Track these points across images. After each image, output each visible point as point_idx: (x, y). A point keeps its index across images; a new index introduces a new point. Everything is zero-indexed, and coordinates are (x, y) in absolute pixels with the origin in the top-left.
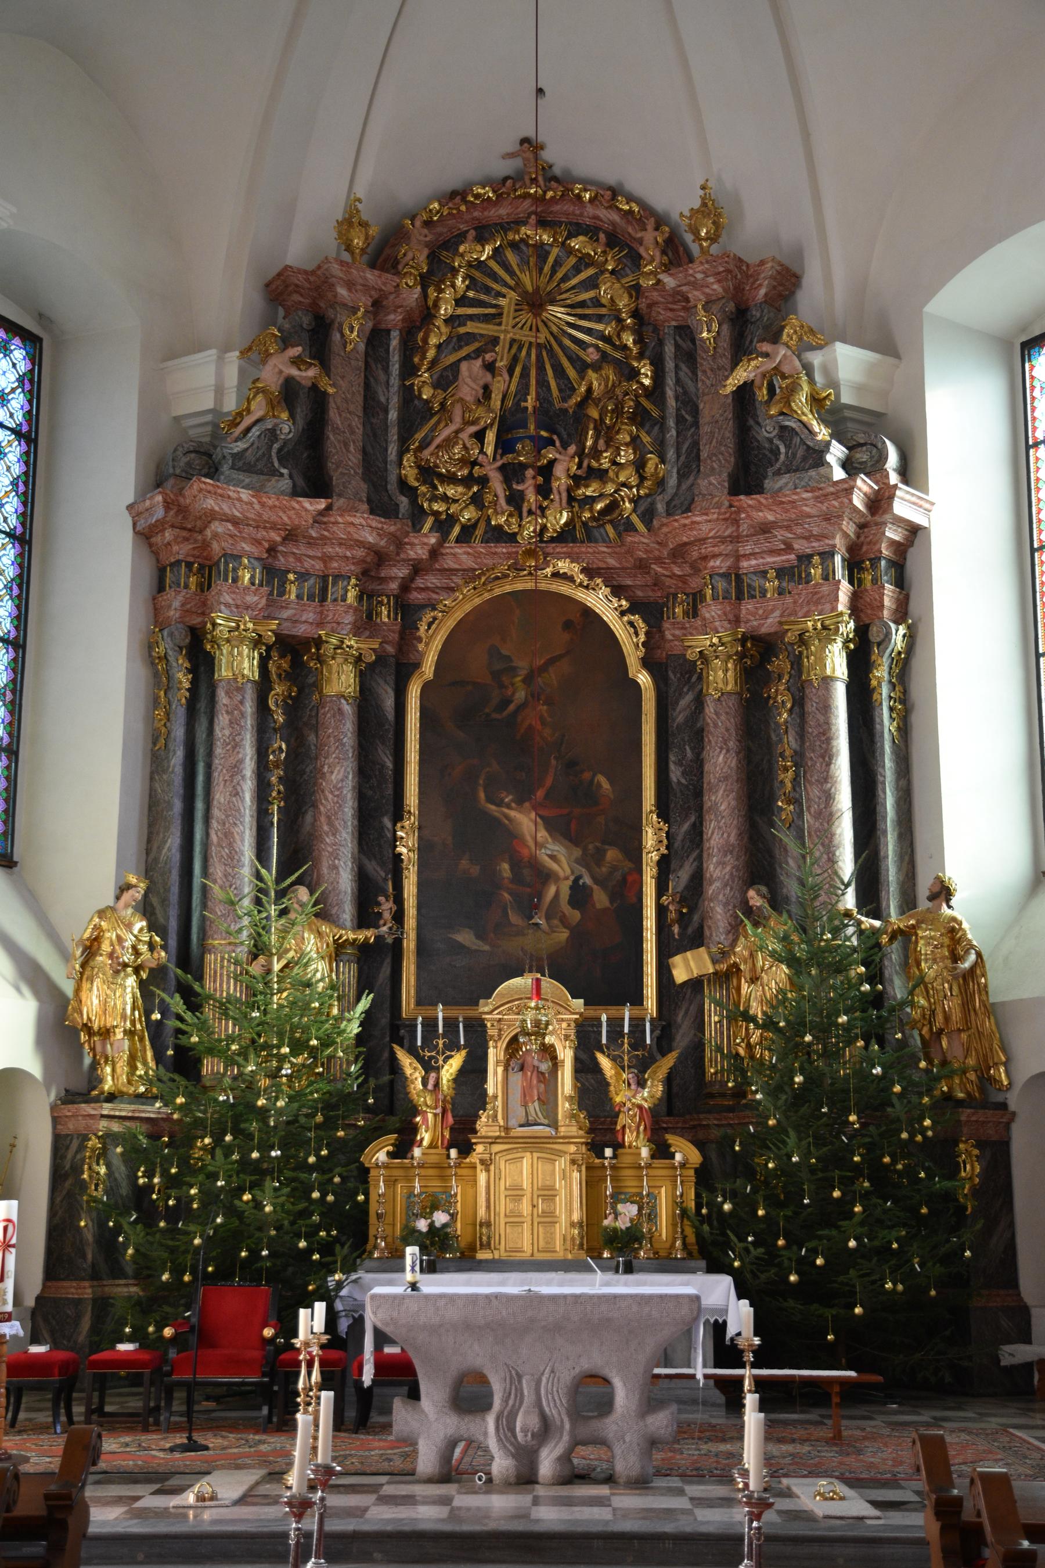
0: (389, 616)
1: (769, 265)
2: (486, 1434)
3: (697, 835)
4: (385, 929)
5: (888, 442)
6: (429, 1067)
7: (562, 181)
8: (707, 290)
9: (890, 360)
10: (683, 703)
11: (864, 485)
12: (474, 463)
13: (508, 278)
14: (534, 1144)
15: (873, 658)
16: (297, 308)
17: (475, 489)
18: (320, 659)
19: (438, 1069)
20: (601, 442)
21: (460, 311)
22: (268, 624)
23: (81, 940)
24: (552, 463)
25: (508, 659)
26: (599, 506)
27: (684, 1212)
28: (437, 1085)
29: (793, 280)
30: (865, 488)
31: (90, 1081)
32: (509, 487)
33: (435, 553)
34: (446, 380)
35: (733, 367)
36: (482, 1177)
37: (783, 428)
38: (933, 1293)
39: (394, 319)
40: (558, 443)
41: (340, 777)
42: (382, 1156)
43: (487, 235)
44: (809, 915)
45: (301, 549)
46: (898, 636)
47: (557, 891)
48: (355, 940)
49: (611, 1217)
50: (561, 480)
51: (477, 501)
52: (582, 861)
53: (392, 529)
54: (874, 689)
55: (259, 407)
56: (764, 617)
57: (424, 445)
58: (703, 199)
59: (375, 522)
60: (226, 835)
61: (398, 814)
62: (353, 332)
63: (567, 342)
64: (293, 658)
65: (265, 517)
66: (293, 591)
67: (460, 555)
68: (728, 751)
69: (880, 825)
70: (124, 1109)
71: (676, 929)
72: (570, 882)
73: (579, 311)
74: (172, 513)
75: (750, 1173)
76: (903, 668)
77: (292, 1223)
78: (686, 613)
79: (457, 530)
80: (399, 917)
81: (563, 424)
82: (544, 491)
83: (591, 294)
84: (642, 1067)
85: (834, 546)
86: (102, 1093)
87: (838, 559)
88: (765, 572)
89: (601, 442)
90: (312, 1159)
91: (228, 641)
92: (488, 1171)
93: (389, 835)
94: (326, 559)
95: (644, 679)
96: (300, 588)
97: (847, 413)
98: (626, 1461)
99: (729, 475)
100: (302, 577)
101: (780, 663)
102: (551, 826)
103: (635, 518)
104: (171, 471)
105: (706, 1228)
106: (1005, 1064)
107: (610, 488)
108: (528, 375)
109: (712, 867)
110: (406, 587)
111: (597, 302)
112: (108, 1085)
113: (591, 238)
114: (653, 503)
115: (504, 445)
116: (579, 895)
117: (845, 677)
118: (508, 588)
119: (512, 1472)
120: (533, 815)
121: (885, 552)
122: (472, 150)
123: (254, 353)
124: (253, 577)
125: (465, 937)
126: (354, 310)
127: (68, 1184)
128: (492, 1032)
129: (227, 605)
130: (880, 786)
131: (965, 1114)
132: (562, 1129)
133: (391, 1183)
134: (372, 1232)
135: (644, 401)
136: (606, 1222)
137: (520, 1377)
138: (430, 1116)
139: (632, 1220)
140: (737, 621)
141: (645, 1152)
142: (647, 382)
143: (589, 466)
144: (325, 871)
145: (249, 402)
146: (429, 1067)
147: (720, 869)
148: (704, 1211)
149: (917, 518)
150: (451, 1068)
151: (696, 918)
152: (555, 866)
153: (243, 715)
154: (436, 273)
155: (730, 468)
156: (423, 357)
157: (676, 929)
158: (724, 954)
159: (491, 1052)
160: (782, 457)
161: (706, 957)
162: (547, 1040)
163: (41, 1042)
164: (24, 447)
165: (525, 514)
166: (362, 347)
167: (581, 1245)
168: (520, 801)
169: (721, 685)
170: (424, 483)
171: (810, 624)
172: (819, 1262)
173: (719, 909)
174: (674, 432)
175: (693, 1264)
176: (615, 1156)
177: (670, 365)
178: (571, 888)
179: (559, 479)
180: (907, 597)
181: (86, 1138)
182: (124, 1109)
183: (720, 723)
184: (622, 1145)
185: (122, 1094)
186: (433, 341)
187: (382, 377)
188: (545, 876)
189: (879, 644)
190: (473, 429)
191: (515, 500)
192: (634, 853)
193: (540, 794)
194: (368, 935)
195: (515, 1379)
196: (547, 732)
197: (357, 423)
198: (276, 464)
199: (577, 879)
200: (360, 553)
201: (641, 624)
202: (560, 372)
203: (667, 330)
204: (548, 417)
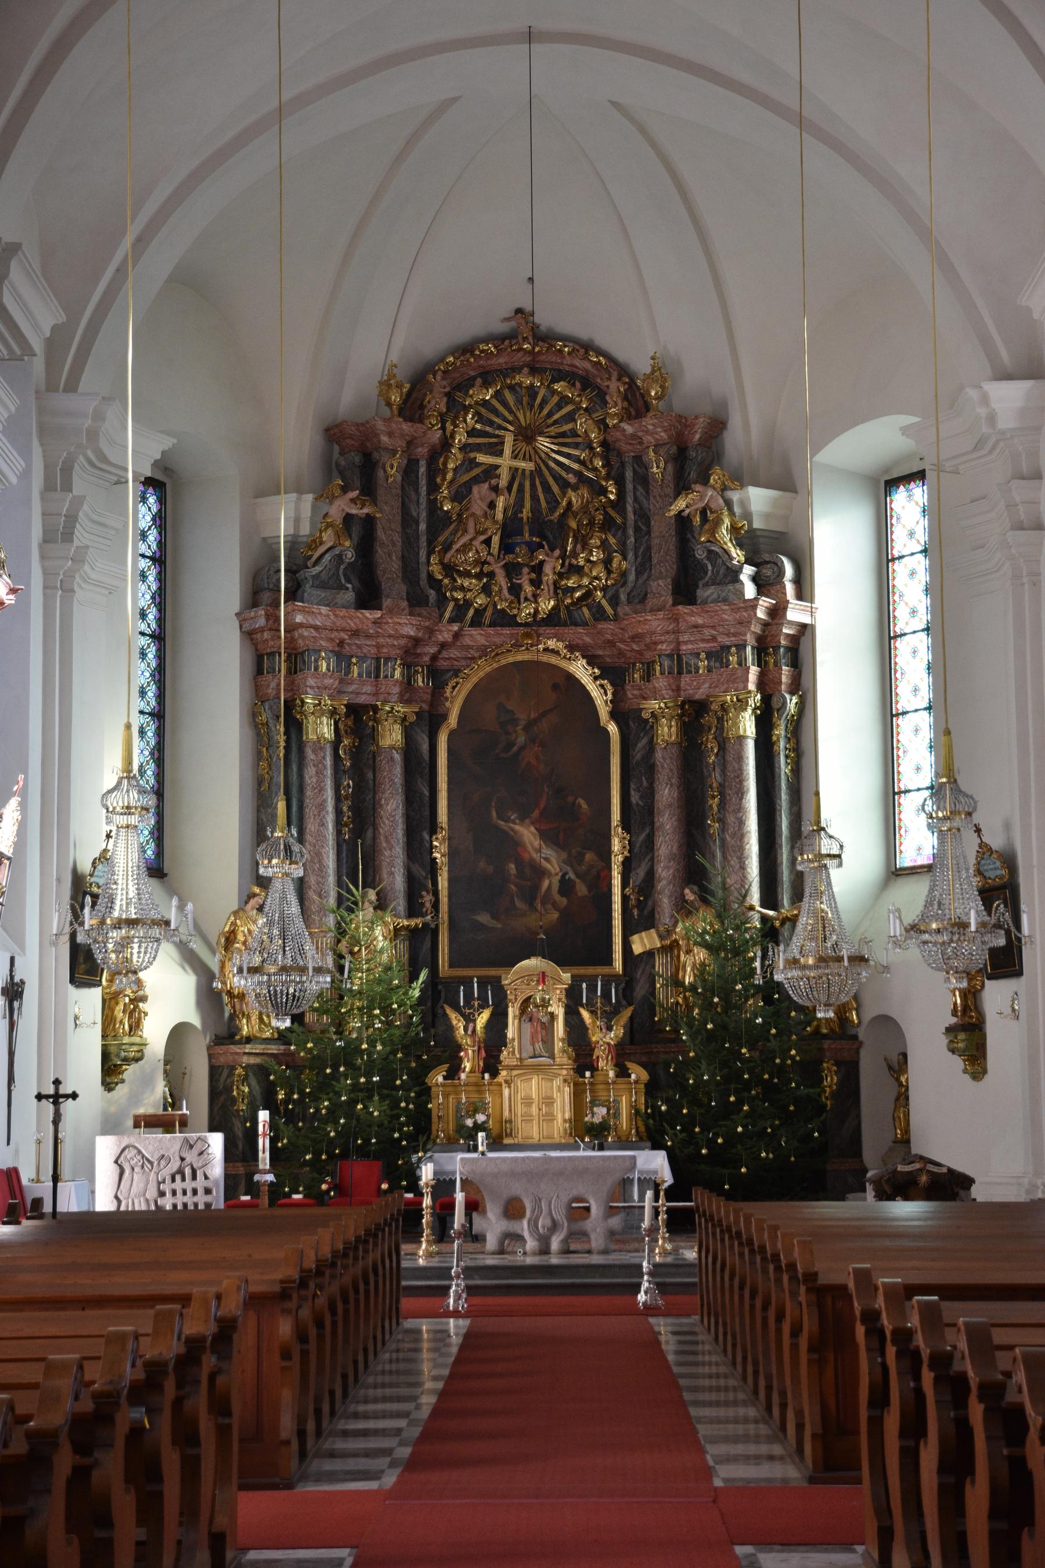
0: (423, 682)
1: (702, 420)
2: (523, 1229)
4: (429, 917)
5: (784, 559)
6: (469, 1019)
7: (545, 338)
8: (656, 436)
9: (787, 494)
10: (640, 745)
11: (765, 602)
13: (506, 414)
14: (537, 1069)
15: (774, 720)
16: (349, 456)
17: (485, 580)
18: (377, 721)
19: (474, 1021)
20: (579, 546)
21: (471, 441)
22: (341, 700)
23: (223, 933)
25: (512, 712)
26: (578, 594)
27: (637, 1112)
28: (474, 1031)
30: (766, 604)
31: (229, 1028)
32: (510, 580)
33: (457, 636)
34: (461, 495)
35: (676, 498)
36: (506, 1092)
37: (710, 552)
38: (793, 1159)
39: (422, 451)
40: (546, 547)
41: (394, 806)
42: (440, 1079)
43: (490, 379)
44: (728, 910)
46: (792, 703)
47: (550, 884)
48: (408, 926)
49: (589, 1116)
50: (549, 576)
51: (486, 590)
52: (568, 862)
53: (427, 624)
54: (774, 743)
57: (447, 548)
58: (653, 367)
59: (415, 620)
60: (316, 854)
61: (434, 828)
62: (392, 470)
63: (552, 464)
64: (358, 721)
65: (338, 623)
67: (476, 637)
68: (671, 786)
69: (778, 840)
70: (258, 1048)
71: (636, 912)
72: (559, 877)
73: (561, 440)
74: (271, 622)
75: (683, 1087)
77: (390, 1122)
78: (642, 678)
79: (471, 612)
80: (436, 905)
81: (549, 532)
82: (536, 583)
83: (570, 426)
84: (609, 1017)
85: (746, 641)
86: (242, 1038)
87: (749, 649)
88: (699, 654)
89: (579, 546)
90: (398, 1082)
91: (313, 713)
92: (509, 1087)
93: (428, 845)
94: (378, 647)
95: (612, 728)
97: (758, 533)
98: (597, 1241)
99: (673, 580)
101: (708, 719)
102: (543, 835)
103: (604, 602)
104: (266, 585)
105: (651, 1121)
106: (857, 1010)
107: (585, 581)
108: (523, 491)
109: (660, 870)
110: (434, 658)
111: (574, 433)
112: (245, 1031)
113: (569, 382)
114: (617, 591)
115: (506, 548)
116: (566, 887)
117: (754, 735)
118: (511, 660)
119: (537, 1248)
120: (532, 829)
121: (783, 642)
122: (483, 315)
123: (324, 495)
124: (328, 665)
125: (484, 918)
126: (394, 452)
127: (222, 1099)
128: (510, 997)
129: (311, 687)
130: (778, 813)
131: (826, 1044)
132: (558, 1060)
133: (446, 1096)
134: (434, 1127)
135: (610, 510)
136: (586, 1119)
137: (540, 1200)
138: (470, 1052)
139: (603, 1117)
140: (678, 689)
141: (611, 1074)
142: (612, 497)
144: (385, 876)
145: (321, 533)
147: (665, 872)
148: (649, 1111)
150: (483, 1018)
151: (650, 903)
152: (548, 866)
153: (325, 767)
154: (455, 409)
155: (673, 573)
156: (444, 479)
157: (636, 912)
158: (669, 932)
159: (510, 1010)
160: (710, 573)
161: (655, 936)
162: (549, 1009)
163: (199, 1004)
164: (157, 723)
165: (522, 600)
166: (399, 478)
167: (571, 1134)
168: (522, 819)
169: (666, 738)
170: (446, 576)
171: (729, 698)
172: (720, 1141)
173: (665, 900)
174: (632, 539)
175: (643, 1144)
176: (592, 1076)
177: (629, 486)
178: (560, 881)
179: (548, 575)
180: (800, 674)
181: (233, 1068)
182: (258, 1048)
183: (666, 764)
184: (597, 1069)
185: (256, 1038)
186: (451, 466)
187: (414, 496)
188: (541, 873)
189: (778, 710)
190: (482, 538)
191: (515, 590)
192: (606, 855)
193: (536, 814)
194: (418, 922)
195: (537, 1201)
197: (397, 538)
198: (343, 581)
199: (564, 876)
201: (609, 687)
202: (547, 488)
203: (628, 458)
204: (538, 525)
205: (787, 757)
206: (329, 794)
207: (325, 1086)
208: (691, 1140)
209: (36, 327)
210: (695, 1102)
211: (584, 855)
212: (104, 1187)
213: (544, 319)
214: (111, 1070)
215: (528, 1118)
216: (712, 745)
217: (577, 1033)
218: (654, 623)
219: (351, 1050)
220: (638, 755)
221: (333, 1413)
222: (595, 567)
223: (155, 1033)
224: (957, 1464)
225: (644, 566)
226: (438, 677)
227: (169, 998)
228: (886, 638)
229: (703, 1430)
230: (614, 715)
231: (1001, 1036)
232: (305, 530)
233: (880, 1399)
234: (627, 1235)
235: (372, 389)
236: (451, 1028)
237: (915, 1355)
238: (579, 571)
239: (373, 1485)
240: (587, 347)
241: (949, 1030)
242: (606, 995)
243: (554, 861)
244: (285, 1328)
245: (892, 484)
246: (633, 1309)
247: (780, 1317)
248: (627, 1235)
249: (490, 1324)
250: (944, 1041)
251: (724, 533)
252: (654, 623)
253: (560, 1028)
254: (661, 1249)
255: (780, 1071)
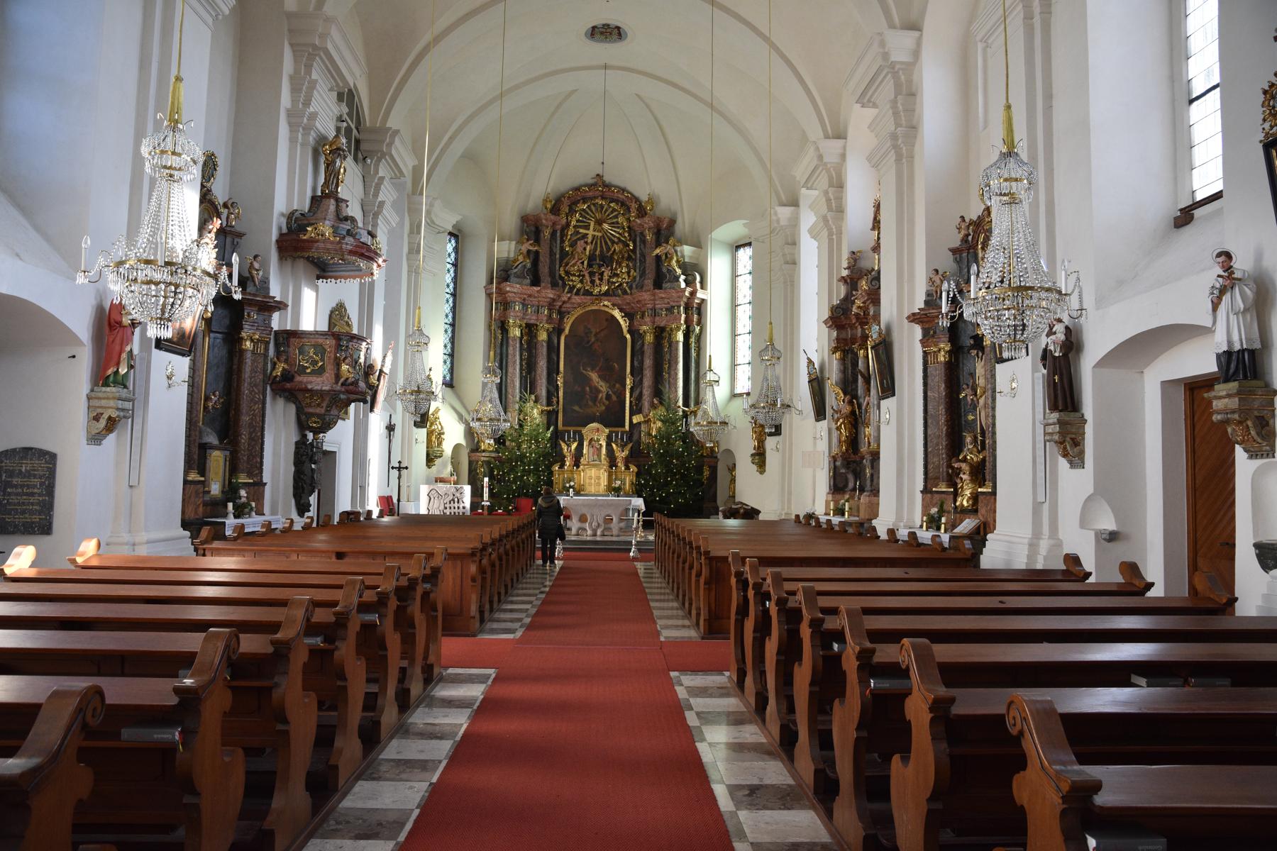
3: (641, 381)
6: (569, 446)
7: (607, 186)
11: (689, 289)
14: (594, 466)
16: (530, 227)
34: (573, 245)
39: (559, 227)
44: (671, 407)
46: (697, 329)
47: (602, 396)
50: (606, 277)
51: (581, 282)
55: (521, 258)
56: (661, 322)
62: (547, 233)
64: (530, 330)
67: (577, 299)
75: (650, 474)
76: (700, 338)
81: (606, 260)
82: (601, 279)
84: (623, 447)
95: (628, 336)
98: (615, 532)
102: (600, 377)
115: (590, 265)
116: (608, 397)
122: (581, 174)
123: (519, 242)
125: (576, 408)
146: (569, 446)
147: (647, 393)
150: (574, 446)
154: (572, 211)
188: (599, 391)
191: (593, 282)
192: (624, 385)
204: (603, 257)
206: (518, 357)
207: (512, 469)
208: (653, 494)
209: (405, 165)
210: (654, 480)
212: (422, 503)
213: (607, 179)
214: (430, 460)
215: (590, 484)
216: (666, 344)
217: (610, 453)
218: (646, 296)
219: (523, 456)
220: (638, 347)
221: (499, 601)
222: (623, 274)
223: (447, 448)
224: (791, 650)
225: (643, 274)
226: (562, 314)
227: (453, 434)
228: (734, 306)
229: (656, 613)
230: (629, 331)
231: (772, 458)
232: (512, 255)
233: (743, 611)
234: (627, 529)
235: (540, 202)
236: (562, 449)
237: (746, 582)
238: (617, 275)
239: (511, 636)
240: (624, 190)
242: (622, 439)
244: (473, 569)
245: (738, 247)
246: (628, 559)
247: (691, 567)
248: (627, 529)
249: (571, 563)
251: (674, 263)
252: (646, 296)
253: (604, 450)
254: (639, 536)
255: (688, 469)
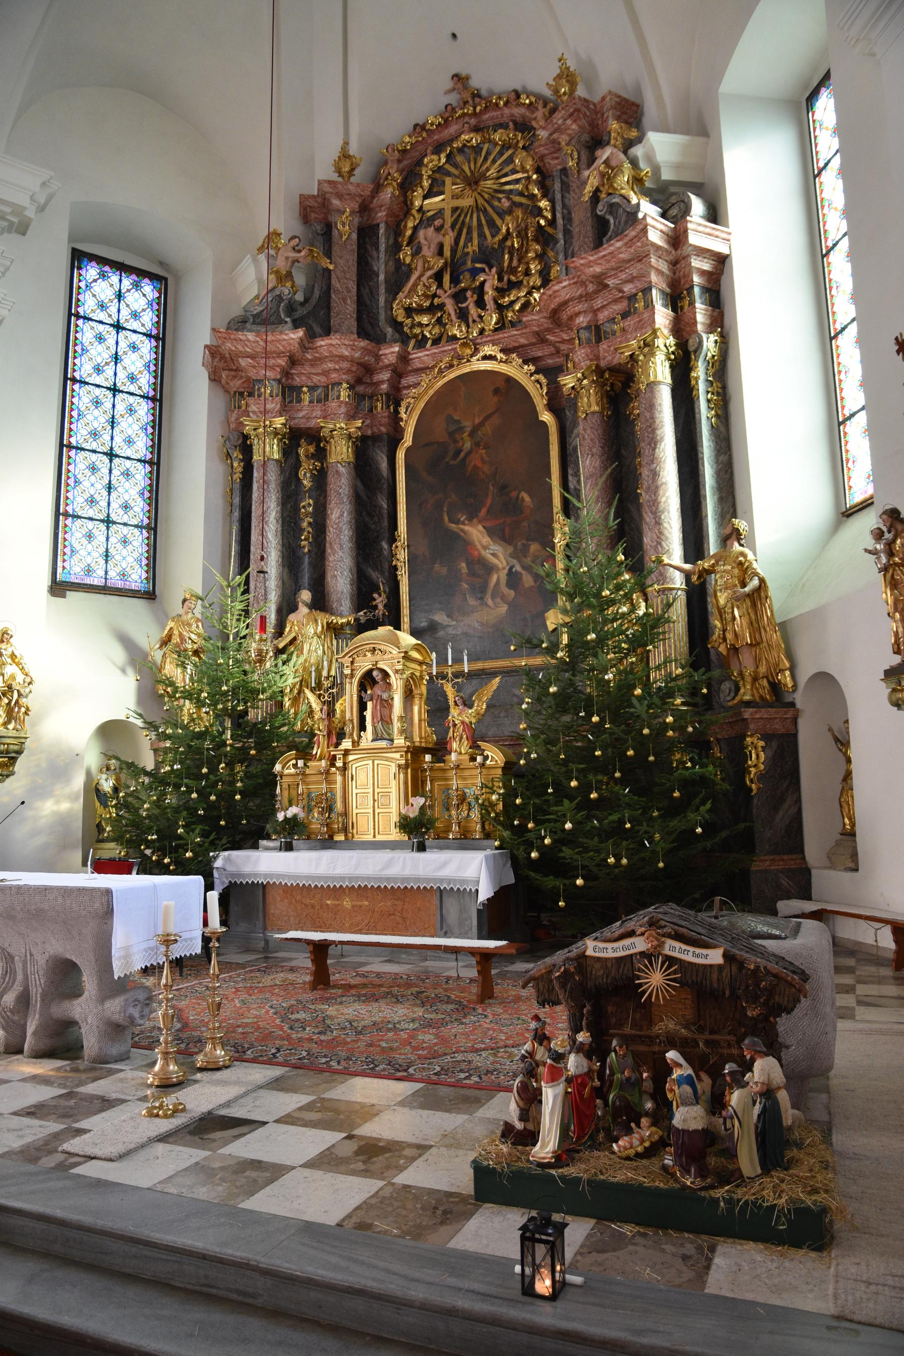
8: (570, 132)
9: (700, 140)
12: (435, 296)
24: (483, 284)
25: (459, 422)
29: (634, 108)
45: (307, 369)
46: (710, 344)
47: (498, 578)
50: (490, 293)
56: (614, 353)
66: (306, 398)
69: (702, 493)
72: (506, 571)
82: (481, 303)
94: (326, 373)
96: (311, 395)
97: (672, 189)
100: (312, 389)
102: (490, 532)
116: (513, 579)
120: (480, 527)
143: (509, 280)
149: (723, 249)
152: (495, 561)
163: (140, 701)
168: (470, 519)
174: (562, 242)
187: (375, 254)
188: (489, 569)
189: (695, 351)
191: (463, 315)
193: (483, 512)
196: (486, 468)
200: (345, 365)
201: (544, 381)
205: (709, 401)
211: (529, 546)
213: (491, 79)
241: (890, 674)
243: (501, 556)
250: (884, 690)
